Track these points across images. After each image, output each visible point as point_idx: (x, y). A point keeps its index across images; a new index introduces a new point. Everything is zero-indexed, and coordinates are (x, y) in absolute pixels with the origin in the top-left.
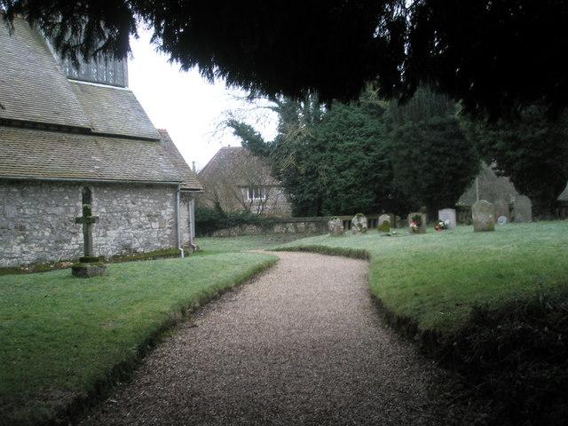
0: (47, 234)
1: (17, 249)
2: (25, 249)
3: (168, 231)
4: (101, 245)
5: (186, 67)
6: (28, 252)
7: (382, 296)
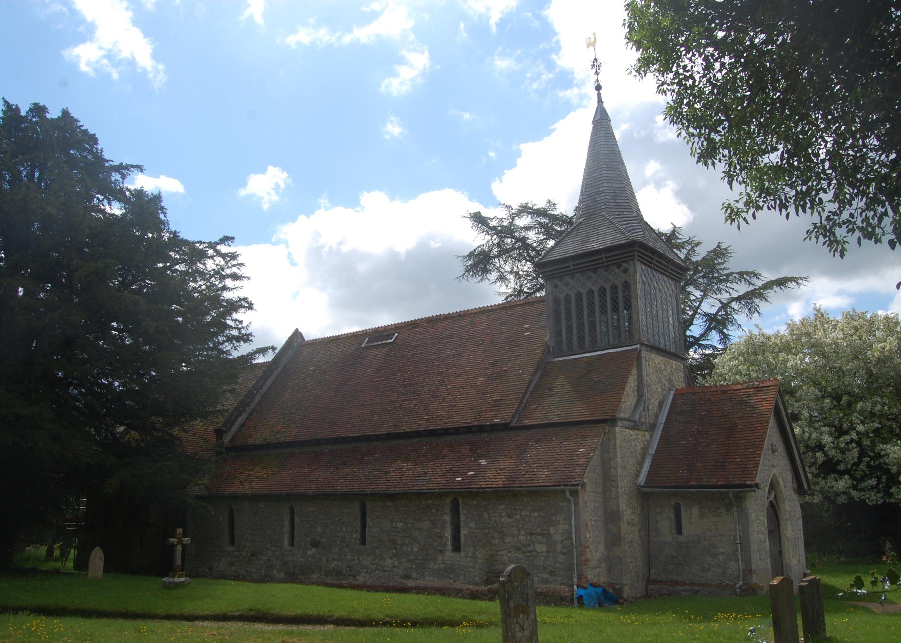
0: (416, 549)
1: (389, 562)
2: (397, 564)
3: (561, 558)
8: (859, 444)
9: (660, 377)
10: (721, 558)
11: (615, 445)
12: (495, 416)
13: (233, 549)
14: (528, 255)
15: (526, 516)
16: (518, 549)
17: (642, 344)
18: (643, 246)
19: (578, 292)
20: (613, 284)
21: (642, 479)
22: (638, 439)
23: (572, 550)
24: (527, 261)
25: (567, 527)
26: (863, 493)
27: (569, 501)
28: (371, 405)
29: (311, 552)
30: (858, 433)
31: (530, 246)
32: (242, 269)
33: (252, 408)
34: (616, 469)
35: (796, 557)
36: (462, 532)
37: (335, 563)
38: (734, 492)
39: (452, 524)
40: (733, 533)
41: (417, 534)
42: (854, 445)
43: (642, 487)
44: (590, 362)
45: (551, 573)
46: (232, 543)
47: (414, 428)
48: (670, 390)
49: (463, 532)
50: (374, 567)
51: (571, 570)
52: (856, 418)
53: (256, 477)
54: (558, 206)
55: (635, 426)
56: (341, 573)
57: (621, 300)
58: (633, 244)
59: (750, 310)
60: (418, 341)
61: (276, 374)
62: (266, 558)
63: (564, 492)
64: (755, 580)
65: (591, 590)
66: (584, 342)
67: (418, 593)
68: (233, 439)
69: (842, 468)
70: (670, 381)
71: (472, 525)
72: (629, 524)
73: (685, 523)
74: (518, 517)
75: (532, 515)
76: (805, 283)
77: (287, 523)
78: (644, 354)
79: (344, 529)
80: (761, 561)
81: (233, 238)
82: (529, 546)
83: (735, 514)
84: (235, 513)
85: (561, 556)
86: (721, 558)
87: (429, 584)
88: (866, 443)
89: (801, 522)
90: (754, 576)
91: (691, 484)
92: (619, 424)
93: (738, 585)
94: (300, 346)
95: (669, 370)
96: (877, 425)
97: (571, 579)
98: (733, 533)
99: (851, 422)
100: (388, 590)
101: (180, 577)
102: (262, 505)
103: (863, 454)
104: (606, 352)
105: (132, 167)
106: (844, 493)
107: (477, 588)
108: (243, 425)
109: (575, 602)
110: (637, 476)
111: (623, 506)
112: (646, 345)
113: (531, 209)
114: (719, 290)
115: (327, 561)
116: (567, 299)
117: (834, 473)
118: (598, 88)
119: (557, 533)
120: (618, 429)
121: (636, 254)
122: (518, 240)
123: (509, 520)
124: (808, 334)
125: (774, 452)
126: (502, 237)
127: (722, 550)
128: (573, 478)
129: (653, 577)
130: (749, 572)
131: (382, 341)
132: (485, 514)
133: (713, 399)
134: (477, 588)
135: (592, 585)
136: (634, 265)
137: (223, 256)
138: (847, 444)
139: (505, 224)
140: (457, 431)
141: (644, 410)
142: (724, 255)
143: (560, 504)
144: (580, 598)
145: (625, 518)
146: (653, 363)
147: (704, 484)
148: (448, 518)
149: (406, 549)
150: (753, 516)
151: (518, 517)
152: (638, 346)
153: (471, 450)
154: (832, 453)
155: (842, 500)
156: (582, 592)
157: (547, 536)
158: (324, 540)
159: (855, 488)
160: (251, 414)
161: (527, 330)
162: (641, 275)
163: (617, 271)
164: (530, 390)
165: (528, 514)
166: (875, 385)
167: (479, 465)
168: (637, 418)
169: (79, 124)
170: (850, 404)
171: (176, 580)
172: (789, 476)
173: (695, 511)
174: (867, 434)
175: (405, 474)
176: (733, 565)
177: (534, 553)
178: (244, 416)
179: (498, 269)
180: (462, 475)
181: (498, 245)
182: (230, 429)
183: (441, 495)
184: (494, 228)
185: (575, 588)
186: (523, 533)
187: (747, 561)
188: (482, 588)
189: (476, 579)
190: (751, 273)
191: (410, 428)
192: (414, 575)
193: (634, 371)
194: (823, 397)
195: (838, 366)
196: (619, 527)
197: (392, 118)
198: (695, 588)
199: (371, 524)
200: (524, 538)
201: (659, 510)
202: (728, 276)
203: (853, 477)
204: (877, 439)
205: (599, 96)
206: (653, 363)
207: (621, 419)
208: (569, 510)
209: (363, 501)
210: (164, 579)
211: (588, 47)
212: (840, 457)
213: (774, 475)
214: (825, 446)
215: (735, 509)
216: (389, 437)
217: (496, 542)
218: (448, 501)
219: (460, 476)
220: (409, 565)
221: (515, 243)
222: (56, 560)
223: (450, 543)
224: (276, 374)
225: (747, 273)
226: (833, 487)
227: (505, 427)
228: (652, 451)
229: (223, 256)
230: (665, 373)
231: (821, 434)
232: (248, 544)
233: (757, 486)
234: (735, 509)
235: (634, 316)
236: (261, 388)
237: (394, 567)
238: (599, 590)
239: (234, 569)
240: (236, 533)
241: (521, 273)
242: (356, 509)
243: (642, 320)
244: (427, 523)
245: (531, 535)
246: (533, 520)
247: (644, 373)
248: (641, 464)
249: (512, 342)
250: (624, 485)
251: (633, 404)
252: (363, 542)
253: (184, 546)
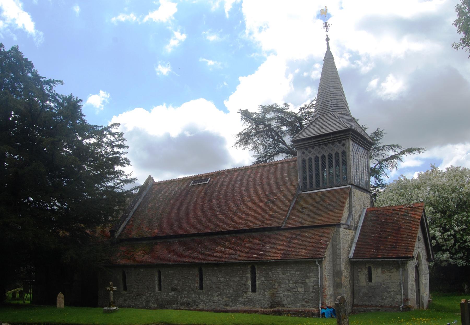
0: (231, 291)
1: (216, 298)
2: (220, 299)
3: (312, 294)
4: (260, 300)
5: (31, 62)
6: (221, 300)
7: (341, 64)
8: (454, 236)
9: (360, 202)
10: (392, 293)
11: (340, 238)
12: (273, 223)
13: (126, 293)
14: (272, 135)
15: (293, 274)
16: (288, 290)
17: (352, 185)
18: (354, 131)
19: (317, 156)
20: (337, 152)
21: (351, 255)
22: (350, 233)
23: (318, 290)
24: (270, 138)
25: (316, 279)
26: (455, 261)
27: (317, 266)
28: (199, 217)
29: (172, 293)
30: (455, 231)
31: (273, 129)
32: (125, 142)
33: (129, 218)
34: (340, 249)
35: (426, 293)
36: (257, 283)
37: (186, 299)
38: (401, 261)
39: (252, 278)
40: (399, 281)
41: (232, 284)
42: (452, 237)
43: (352, 259)
44: (324, 194)
45: (307, 302)
46: (125, 289)
47: (227, 229)
48: (364, 209)
49: (258, 282)
50: (208, 301)
51: (318, 300)
52: (454, 223)
53: (137, 255)
54: (290, 107)
55: (348, 228)
56: (189, 304)
57: (343, 160)
58: (349, 130)
59: (392, 165)
60: (223, 182)
61: (140, 200)
62: (145, 297)
63: (315, 262)
64: (410, 304)
65: (328, 310)
66: (319, 184)
67: (248, 313)
68: (120, 235)
69: (445, 248)
70: (364, 204)
71: (263, 279)
72: (345, 277)
73: (373, 276)
74: (289, 274)
75: (297, 273)
76: (423, 151)
77: (157, 279)
79: (190, 282)
80: (412, 295)
81: (119, 124)
82: (295, 288)
83: (401, 271)
84: (126, 274)
85: (312, 293)
86: (392, 293)
87: (240, 309)
88: (458, 236)
89: (428, 275)
90: (409, 302)
91: (378, 257)
92: (342, 227)
93: (401, 306)
94: (152, 185)
95: (363, 198)
96: (465, 227)
97: (318, 304)
98: (399, 281)
99: (451, 225)
100: (216, 311)
101: (113, 307)
102: (142, 270)
103: (456, 241)
105: (57, 81)
106: (446, 261)
107: (266, 310)
108: (125, 228)
109: (321, 316)
110: (349, 253)
111: (343, 268)
113: (275, 108)
114: (378, 155)
115: (181, 298)
116: (310, 159)
117: (441, 251)
118: (328, 40)
119: (310, 282)
120: (341, 229)
121: (350, 136)
122: (266, 126)
123: (283, 276)
124: (430, 180)
125: (419, 240)
126: (258, 124)
127: (393, 289)
128: (320, 254)
129: (355, 303)
130: (407, 300)
131: (201, 182)
132: (270, 273)
133: (388, 213)
134: (266, 310)
135: (328, 307)
136: (349, 142)
137: (113, 134)
138: (448, 236)
139: (260, 117)
140: (251, 231)
141: (352, 219)
142: (380, 135)
143: (312, 268)
144: (323, 314)
145: (344, 274)
146: (356, 193)
147: (386, 257)
148: (249, 275)
149: (225, 291)
150: (410, 272)
151: (289, 274)
152: (350, 186)
153: (260, 240)
154: (441, 241)
155: (445, 264)
156: (324, 311)
157: (305, 283)
158: (179, 288)
159: (451, 258)
160: (128, 222)
161: (286, 177)
163: (339, 145)
164: (291, 209)
165: (294, 272)
166: (464, 206)
167: (266, 248)
168: (349, 223)
169: (22, 55)
170: (450, 216)
171: (112, 308)
172: (424, 252)
173: (379, 270)
174: (459, 231)
175: (222, 252)
176: (398, 296)
177: (297, 292)
178: (125, 223)
179: (254, 143)
180: (257, 253)
181: (255, 129)
182: (118, 230)
183: (244, 264)
184: (253, 119)
185: (320, 309)
186: (291, 282)
187: (406, 295)
188: (269, 310)
189: (266, 305)
190: (396, 145)
191: (224, 229)
192: (231, 304)
193: (348, 199)
194: (436, 212)
195: (446, 196)
196: (341, 279)
198: (378, 308)
199: (205, 279)
200: (292, 285)
201: (360, 270)
202: (384, 146)
203: (450, 253)
204: (464, 234)
205: (328, 44)
206: (356, 193)
207: (343, 224)
208: (317, 270)
209: (201, 268)
210: (105, 308)
212: (444, 243)
213: (419, 252)
214: (436, 237)
215: (401, 269)
216: (212, 234)
217: (276, 287)
218: (249, 267)
219: (256, 254)
220: (228, 299)
221: (265, 128)
222: (18, 299)
223: (250, 288)
224: (140, 200)
225: (394, 146)
226: (440, 258)
227: (279, 228)
228: (356, 240)
229: (113, 134)
231: (435, 231)
232: (135, 290)
233: (413, 257)
234: (401, 269)
235: (348, 169)
236: (133, 208)
237: (219, 300)
238: (331, 310)
239: (127, 302)
240: (127, 285)
241: (266, 145)
242: (197, 272)
243: (353, 171)
244: (238, 278)
245: (296, 283)
246: (297, 276)
247: (353, 200)
248: (350, 247)
249: (277, 183)
250: (343, 258)
251: (347, 216)
252: (201, 288)
253: (114, 291)
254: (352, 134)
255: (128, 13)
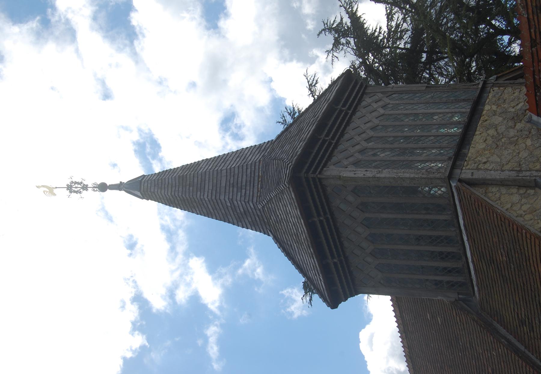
17: (450, 176)
48: (530, 121)
70: (516, 118)
78: (466, 174)
95: (497, 119)
104: (463, 228)
112: (453, 167)
118: (103, 187)
162: (342, 170)
197: (352, 41)
205: (114, 187)
211: (55, 195)
230: (502, 129)
254: (307, 172)
255: (206, 339)
